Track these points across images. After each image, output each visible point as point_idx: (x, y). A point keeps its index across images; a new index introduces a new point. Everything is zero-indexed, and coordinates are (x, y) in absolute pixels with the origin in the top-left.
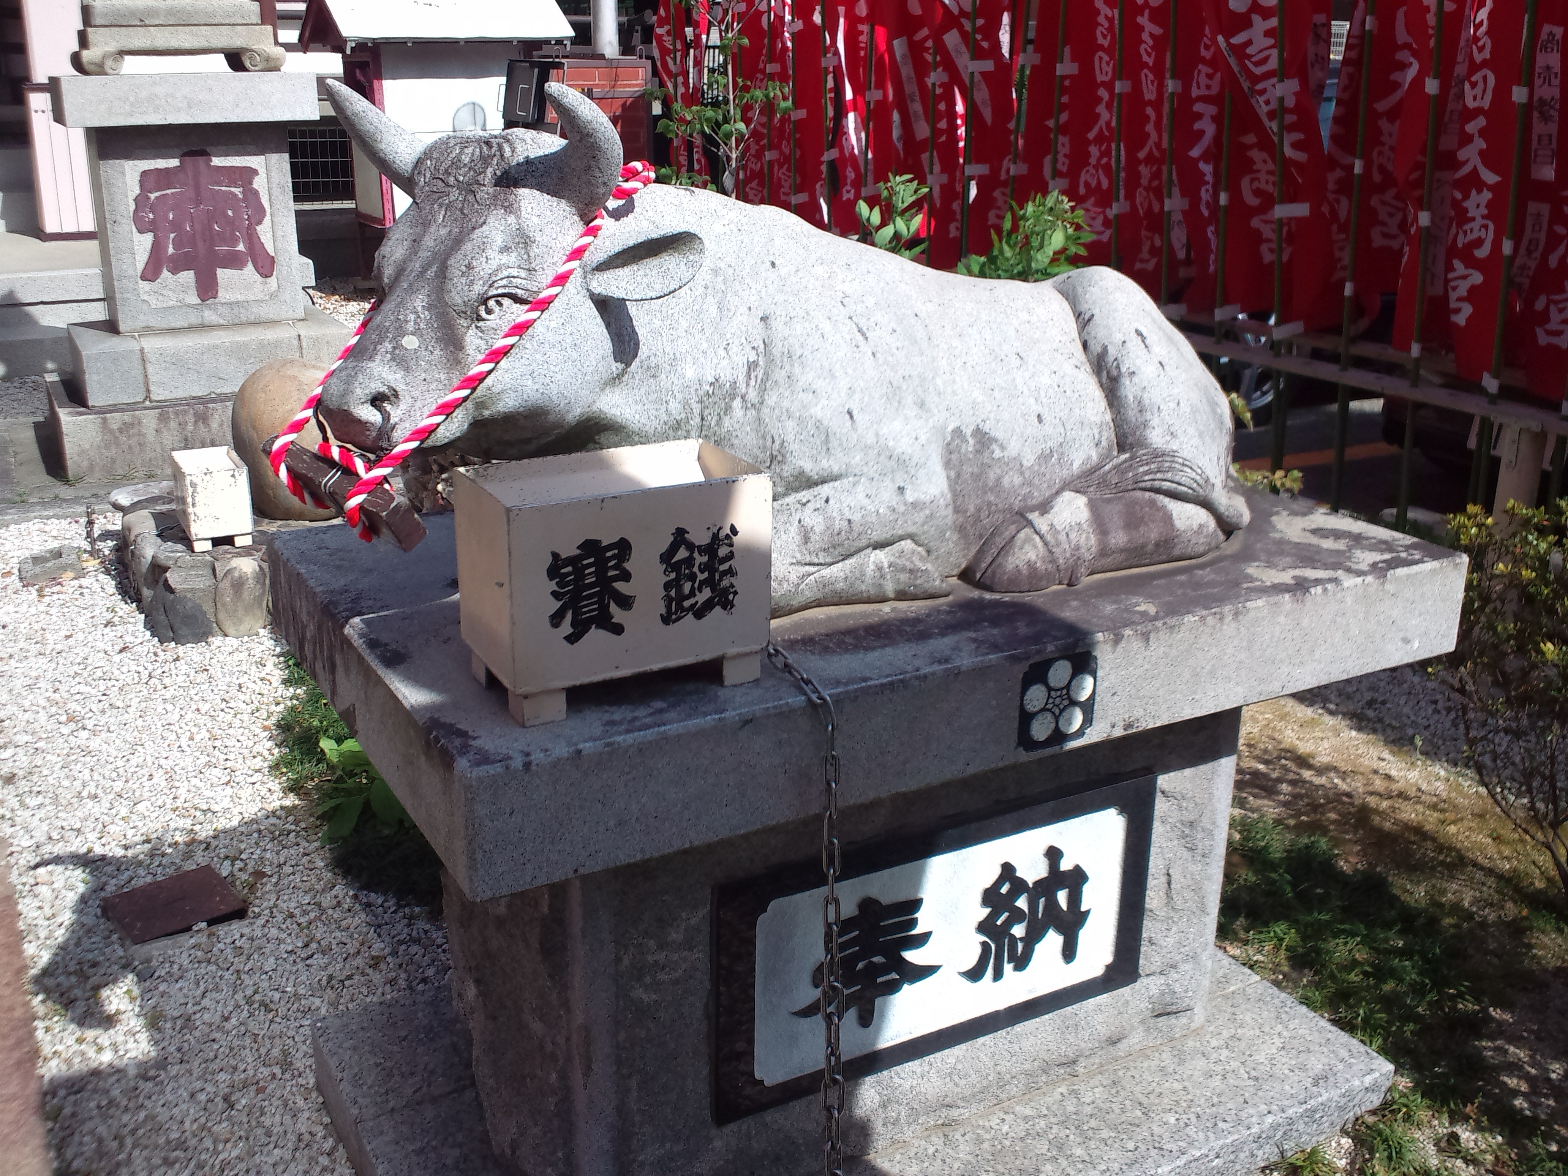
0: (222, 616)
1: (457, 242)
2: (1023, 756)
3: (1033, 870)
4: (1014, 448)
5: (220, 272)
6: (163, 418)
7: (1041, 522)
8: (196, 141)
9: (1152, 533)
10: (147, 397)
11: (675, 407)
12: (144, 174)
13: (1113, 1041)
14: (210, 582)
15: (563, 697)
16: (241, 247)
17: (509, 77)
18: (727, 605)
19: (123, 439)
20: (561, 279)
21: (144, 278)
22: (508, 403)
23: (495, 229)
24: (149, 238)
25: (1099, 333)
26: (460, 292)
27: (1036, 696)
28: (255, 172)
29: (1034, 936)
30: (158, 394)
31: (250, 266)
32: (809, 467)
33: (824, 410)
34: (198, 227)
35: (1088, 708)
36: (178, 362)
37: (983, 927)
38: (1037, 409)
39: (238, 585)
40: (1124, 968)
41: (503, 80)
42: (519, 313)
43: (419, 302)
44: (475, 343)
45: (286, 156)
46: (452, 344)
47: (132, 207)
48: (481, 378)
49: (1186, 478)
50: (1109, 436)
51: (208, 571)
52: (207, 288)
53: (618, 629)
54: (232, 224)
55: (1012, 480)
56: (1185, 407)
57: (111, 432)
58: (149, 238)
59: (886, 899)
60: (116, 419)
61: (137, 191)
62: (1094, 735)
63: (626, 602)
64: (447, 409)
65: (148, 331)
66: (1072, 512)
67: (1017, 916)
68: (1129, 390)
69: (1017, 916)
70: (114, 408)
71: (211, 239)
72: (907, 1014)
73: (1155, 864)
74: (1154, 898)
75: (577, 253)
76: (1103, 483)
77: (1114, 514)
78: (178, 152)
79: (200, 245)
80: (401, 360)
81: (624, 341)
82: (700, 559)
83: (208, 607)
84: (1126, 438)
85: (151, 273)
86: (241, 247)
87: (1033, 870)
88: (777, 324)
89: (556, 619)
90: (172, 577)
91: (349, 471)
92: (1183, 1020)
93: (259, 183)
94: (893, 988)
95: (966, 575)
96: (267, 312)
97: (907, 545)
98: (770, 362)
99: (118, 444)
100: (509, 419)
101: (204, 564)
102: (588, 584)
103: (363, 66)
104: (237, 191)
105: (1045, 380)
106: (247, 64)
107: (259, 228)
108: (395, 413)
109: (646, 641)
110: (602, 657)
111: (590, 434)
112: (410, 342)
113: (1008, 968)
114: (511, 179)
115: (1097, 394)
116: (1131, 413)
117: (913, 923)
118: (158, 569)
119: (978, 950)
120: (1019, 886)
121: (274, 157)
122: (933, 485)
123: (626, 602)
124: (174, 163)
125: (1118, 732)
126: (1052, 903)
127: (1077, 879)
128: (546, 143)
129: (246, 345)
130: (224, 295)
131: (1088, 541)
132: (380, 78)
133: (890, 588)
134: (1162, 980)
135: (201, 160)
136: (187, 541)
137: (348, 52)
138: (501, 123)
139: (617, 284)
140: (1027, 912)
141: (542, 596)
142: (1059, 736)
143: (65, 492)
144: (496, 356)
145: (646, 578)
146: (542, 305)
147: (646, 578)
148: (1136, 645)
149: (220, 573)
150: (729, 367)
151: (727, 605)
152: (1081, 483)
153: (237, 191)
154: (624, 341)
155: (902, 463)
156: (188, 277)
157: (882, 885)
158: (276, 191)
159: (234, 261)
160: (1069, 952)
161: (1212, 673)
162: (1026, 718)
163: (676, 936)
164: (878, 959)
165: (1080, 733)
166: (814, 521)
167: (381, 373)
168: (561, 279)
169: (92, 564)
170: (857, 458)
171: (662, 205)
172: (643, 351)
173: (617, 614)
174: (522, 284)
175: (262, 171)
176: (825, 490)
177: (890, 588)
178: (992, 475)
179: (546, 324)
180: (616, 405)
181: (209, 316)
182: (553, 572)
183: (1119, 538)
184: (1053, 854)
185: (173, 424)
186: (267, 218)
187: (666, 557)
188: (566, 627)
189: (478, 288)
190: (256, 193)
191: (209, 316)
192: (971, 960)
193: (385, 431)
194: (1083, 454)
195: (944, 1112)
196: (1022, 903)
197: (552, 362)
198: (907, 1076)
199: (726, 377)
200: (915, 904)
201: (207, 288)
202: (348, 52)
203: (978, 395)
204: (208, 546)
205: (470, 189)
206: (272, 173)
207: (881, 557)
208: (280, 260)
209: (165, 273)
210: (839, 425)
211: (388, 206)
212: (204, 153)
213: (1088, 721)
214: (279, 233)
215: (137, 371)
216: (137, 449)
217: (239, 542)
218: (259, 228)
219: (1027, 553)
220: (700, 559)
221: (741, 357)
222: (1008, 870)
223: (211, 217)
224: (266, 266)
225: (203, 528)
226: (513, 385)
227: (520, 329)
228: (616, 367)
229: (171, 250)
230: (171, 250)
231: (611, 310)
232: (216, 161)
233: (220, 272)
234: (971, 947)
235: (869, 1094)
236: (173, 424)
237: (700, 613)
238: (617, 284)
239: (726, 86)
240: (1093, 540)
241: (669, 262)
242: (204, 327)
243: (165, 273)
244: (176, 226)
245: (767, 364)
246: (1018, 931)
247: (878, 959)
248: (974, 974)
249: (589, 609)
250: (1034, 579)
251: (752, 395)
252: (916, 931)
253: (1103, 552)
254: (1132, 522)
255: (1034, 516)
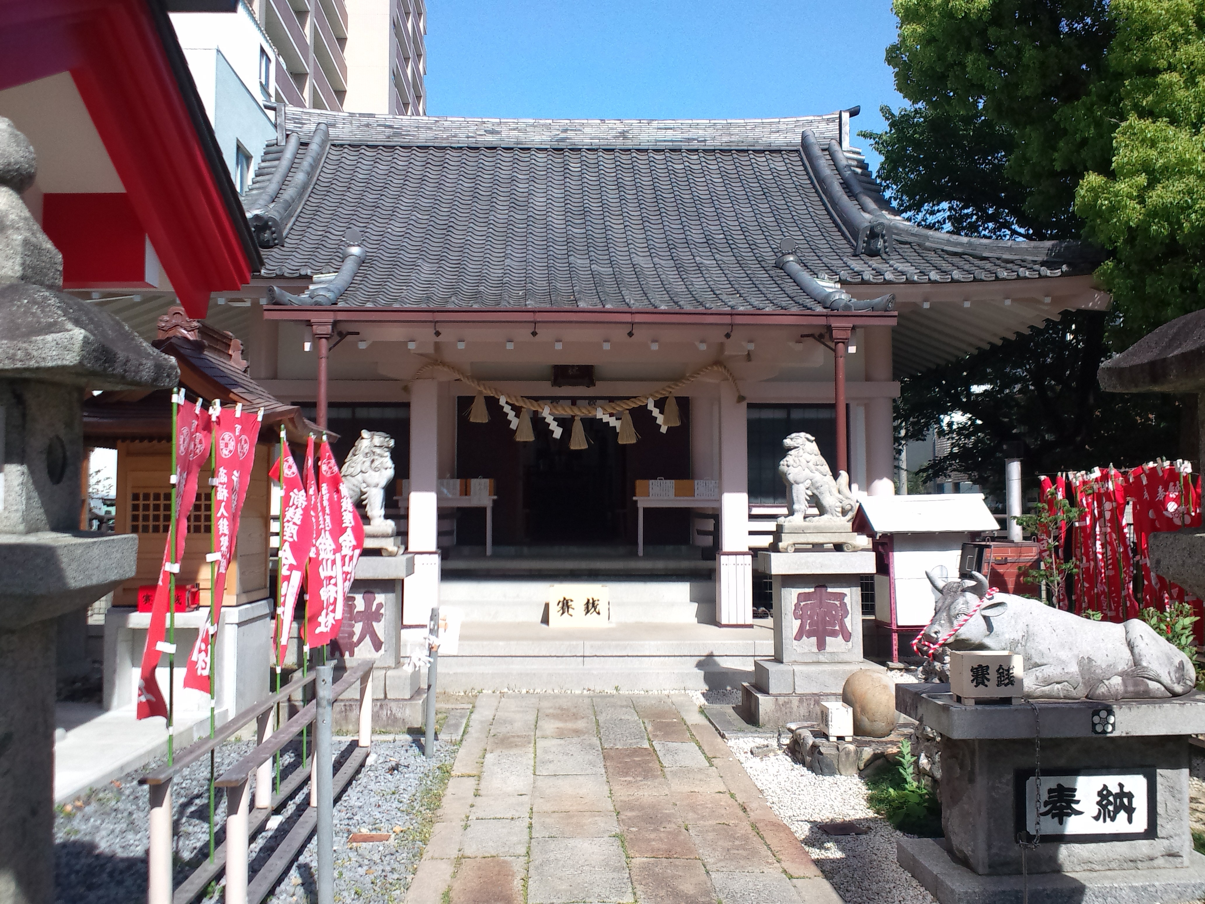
0: (840, 766)
1: (953, 603)
2: (1094, 735)
3: (1115, 790)
4: (1099, 663)
5: (827, 638)
6: (801, 701)
7: (1106, 682)
8: (821, 581)
9: (1142, 688)
10: (794, 692)
11: (1003, 644)
12: (799, 594)
13: (1152, 859)
14: (837, 752)
15: (973, 701)
16: (837, 628)
17: (962, 549)
18: (1013, 684)
19: (783, 709)
20: (975, 611)
21: (795, 639)
22: (963, 637)
23: (961, 600)
24: (799, 621)
25: (1130, 636)
26: (953, 612)
27: (1096, 719)
28: (845, 595)
29: (1116, 811)
30: (799, 691)
31: (841, 636)
32: (1038, 661)
33: (1043, 647)
34: (820, 618)
35: (1113, 725)
36: (808, 677)
37: (1099, 803)
38: (1106, 653)
39: (848, 754)
40: (1151, 833)
41: (959, 552)
42: (966, 617)
43: (945, 614)
44: (956, 623)
45: (860, 588)
46: (951, 623)
47: (793, 608)
48: (956, 630)
49: (1151, 674)
50: (1131, 663)
51: (835, 749)
52: (821, 645)
53: (986, 686)
54: (834, 617)
55: (1099, 671)
56: (1154, 656)
57: (779, 705)
58: (799, 621)
59: (1066, 786)
60: (781, 700)
61: (796, 601)
62: (1116, 734)
63: (988, 680)
64: (950, 635)
65: (795, 662)
66: (1116, 681)
67: (1110, 803)
68: (1136, 650)
69: (1110, 803)
70: (780, 695)
71: (825, 623)
72: (1074, 825)
73: (1159, 798)
74: (1160, 809)
75: (979, 606)
76: (1127, 674)
77: (1130, 682)
78: (814, 585)
79: (820, 626)
80: (941, 626)
81: (990, 627)
82: (1006, 673)
83: (835, 762)
84: (1136, 663)
85: (798, 637)
86: (837, 628)
87: (1115, 790)
88: (1031, 627)
89: (972, 681)
90: (822, 749)
91: (929, 647)
92: (1179, 860)
93: (847, 600)
94: (1069, 815)
95: (1087, 697)
96: (846, 657)
97: (1066, 683)
98: (1028, 635)
99: (781, 711)
100: (963, 641)
101: (834, 746)
102: (980, 674)
103: (883, 544)
104: (838, 603)
105: (1110, 646)
106: (845, 549)
107: (846, 620)
108: (939, 635)
109: (992, 690)
110: (982, 692)
111: (982, 647)
112: (943, 622)
113: (1108, 820)
114: (964, 591)
115: (1128, 652)
116: (1137, 656)
117: (1074, 796)
118: (815, 747)
119: (1097, 811)
120: (1110, 793)
121: (854, 589)
122: (1074, 669)
123: (988, 680)
124: (812, 590)
125: (1124, 735)
126: (1122, 802)
127: (1130, 796)
128: (972, 583)
129: (837, 671)
130: (828, 649)
131: (1121, 689)
132: (893, 551)
133: (1062, 695)
134: (1167, 841)
135: (823, 589)
136: (826, 736)
137: (878, 538)
138: (957, 574)
139: (987, 613)
140: (1113, 804)
141: (969, 676)
142: (1104, 732)
143: (759, 729)
144: (961, 625)
145: (993, 675)
146: (971, 616)
147: (993, 675)
148: (1127, 710)
149: (840, 749)
150: (1018, 636)
151: (1013, 684)
152: (1121, 674)
153: (838, 603)
154: (990, 627)
155: (1064, 662)
156: (814, 639)
157: (1065, 781)
158: (854, 604)
159: (834, 634)
160: (1130, 820)
161: (1154, 723)
162: (1094, 725)
163: (1004, 781)
164: (1064, 804)
165: (1111, 732)
166: (1040, 675)
167: (936, 627)
168: (975, 611)
169: (780, 752)
170: (1051, 660)
171: (999, 597)
172: (995, 630)
173: (986, 682)
174: (966, 611)
175: (849, 594)
176: (1043, 667)
177: (1062, 695)
178: (1093, 669)
179: (971, 620)
180: (987, 641)
181: (822, 658)
182: (972, 670)
183: (1131, 689)
184: (1121, 786)
185: (805, 704)
186: (849, 616)
187: (998, 671)
188: (975, 683)
189: (957, 612)
190: (846, 604)
191: (822, 658)
192: (1095, 813)
193: (937, 639)
194: (1122, 666)
195: (1090, 864)
196: (1111, 798)
197: (973, 629)
198: (1077, 848)
199: (1017, 638)
200: (1075, 790)
201: (821, 645)
202: (878, 538)
203: (1089, 648)
204: (835, 739)
205: (955, 592)
206: (852, 596)
207: (1059, 686)
208: (853, 634)
209: (804, 638)
210: (1046, 652)
211: (893, 616)
212: (825, 586)
213: (1114, 729)
214: (854, 622)
215: (790, 680)
216: (788, 714)
217: (847, 739)
218: (846, 620)
219: (1102, 690)
220: (1006, 673)
221: (1021, 634)
222: (1105, 787)
223: (826, 614)
224: (847, 636)
225: (834, 731)
226: (965, 633)
227: (966, 620)
228: (988, 633)
229: (808, 628)
230: (808, 628)
231: (986, 619)
232: (830, 590)
233: (827, 638)
234: (1095, 810)
235: (1064, 851)
236: (805, 704)
237: (1006, 685)
238: (987, 613)
239: (1052, 563)
240: (1122, 688)
241: (999, 608)
242: (819, 663)
243: (804, 638)
244: (811, 617)
245: (1027, 636)
246: (1111, 808)
247: (1064, 804)
248: (1097, 818)
249: (980, 680)
250: (1104, 697)
251: (1023, 643)
252: (1075, 798)
253: (1126, 692)
254: (1136, 684)
255: (1105, 681)
